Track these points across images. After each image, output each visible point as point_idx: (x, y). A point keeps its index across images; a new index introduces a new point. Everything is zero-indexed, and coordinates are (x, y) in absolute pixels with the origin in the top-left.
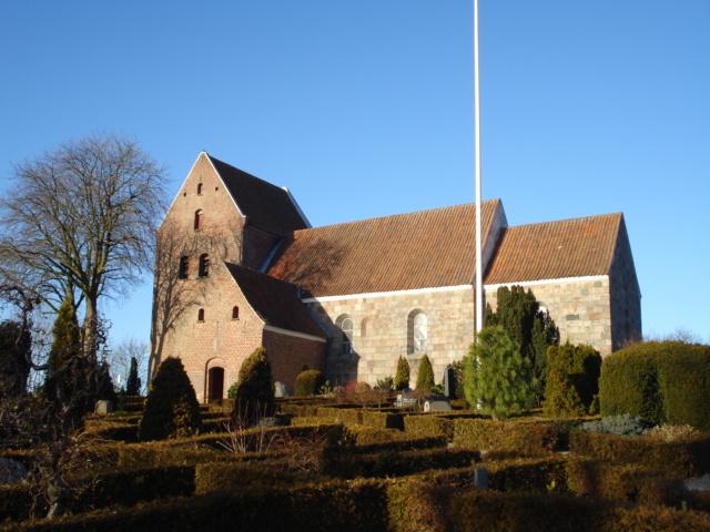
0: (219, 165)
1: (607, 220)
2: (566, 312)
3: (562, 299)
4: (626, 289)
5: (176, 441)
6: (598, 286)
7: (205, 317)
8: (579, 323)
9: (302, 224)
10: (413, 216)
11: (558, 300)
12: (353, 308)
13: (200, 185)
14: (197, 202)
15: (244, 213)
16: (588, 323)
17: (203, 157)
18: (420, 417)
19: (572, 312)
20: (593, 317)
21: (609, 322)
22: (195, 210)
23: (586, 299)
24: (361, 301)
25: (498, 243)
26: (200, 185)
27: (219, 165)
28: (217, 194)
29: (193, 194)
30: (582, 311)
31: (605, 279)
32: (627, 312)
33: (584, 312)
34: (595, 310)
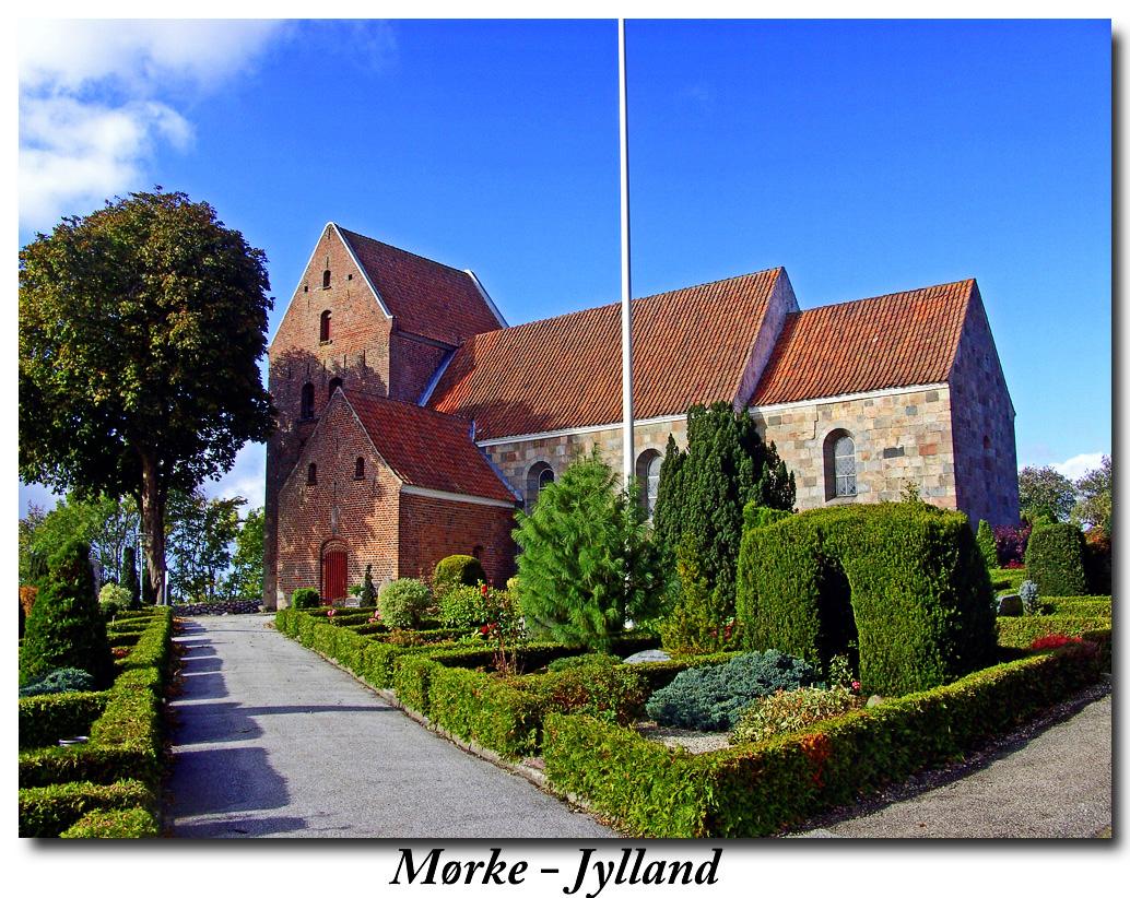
0: (353, 239)
1: (945, 293)
2: (883, 445)
3: (877, 422)
4: (984, 402)
5: (36, 698)
6: (935, 408)
7: (319, 477)
8: (904, 461)
9: (491, 322)
10: (170, 108)
11: (871, 425)
12: (553, 451)
13: (327, 274)
14: (323, 299)
15: (390, 311)
16: (918, 461)
17: (330, 229)
18: (149, 630)
19: (893, 444)
20: (926, 451)
21: (950, 458)
22: (321, 312)
23: (917, 421)
24: (564, 441)
25: (783, 339)
26: (327, 274)
27: (353, 239)
28: (352, 285)
29: (317, 288)
30: (908, 442)
31: (944, 392)
32: (986, 440)
33: (912, 442)
34: (928, 441)
